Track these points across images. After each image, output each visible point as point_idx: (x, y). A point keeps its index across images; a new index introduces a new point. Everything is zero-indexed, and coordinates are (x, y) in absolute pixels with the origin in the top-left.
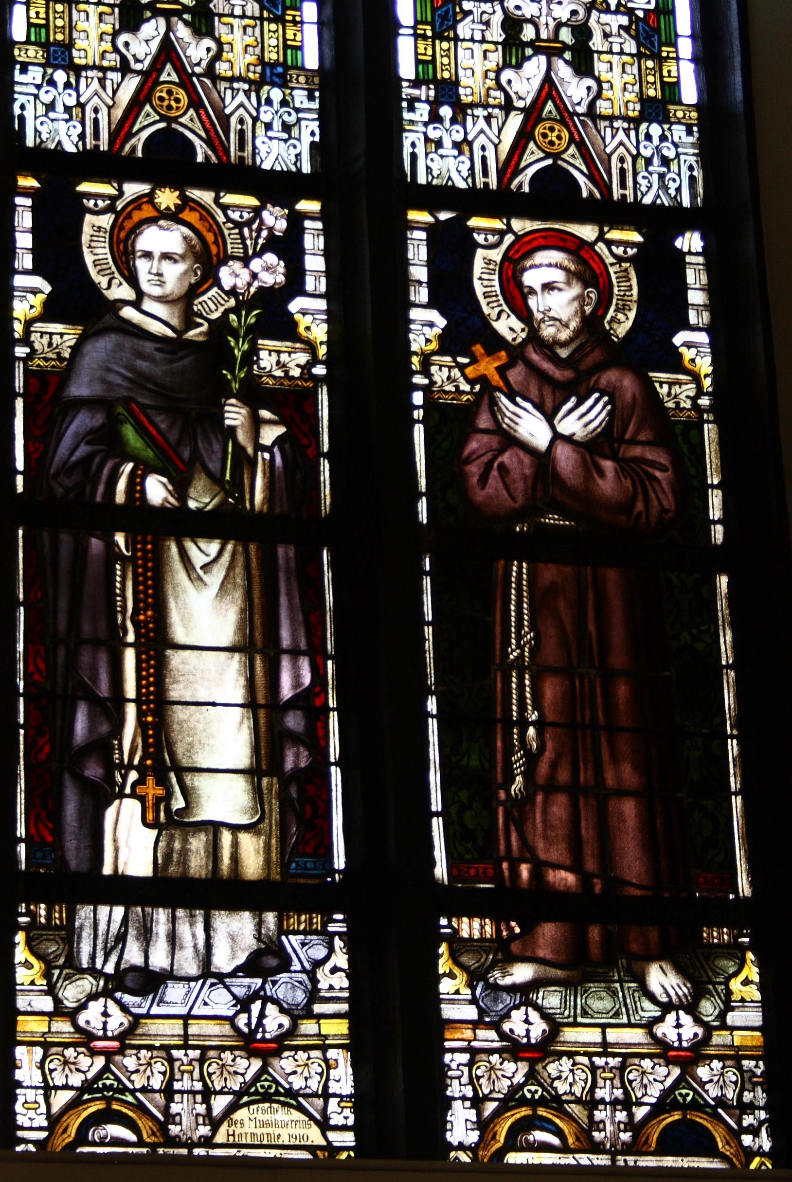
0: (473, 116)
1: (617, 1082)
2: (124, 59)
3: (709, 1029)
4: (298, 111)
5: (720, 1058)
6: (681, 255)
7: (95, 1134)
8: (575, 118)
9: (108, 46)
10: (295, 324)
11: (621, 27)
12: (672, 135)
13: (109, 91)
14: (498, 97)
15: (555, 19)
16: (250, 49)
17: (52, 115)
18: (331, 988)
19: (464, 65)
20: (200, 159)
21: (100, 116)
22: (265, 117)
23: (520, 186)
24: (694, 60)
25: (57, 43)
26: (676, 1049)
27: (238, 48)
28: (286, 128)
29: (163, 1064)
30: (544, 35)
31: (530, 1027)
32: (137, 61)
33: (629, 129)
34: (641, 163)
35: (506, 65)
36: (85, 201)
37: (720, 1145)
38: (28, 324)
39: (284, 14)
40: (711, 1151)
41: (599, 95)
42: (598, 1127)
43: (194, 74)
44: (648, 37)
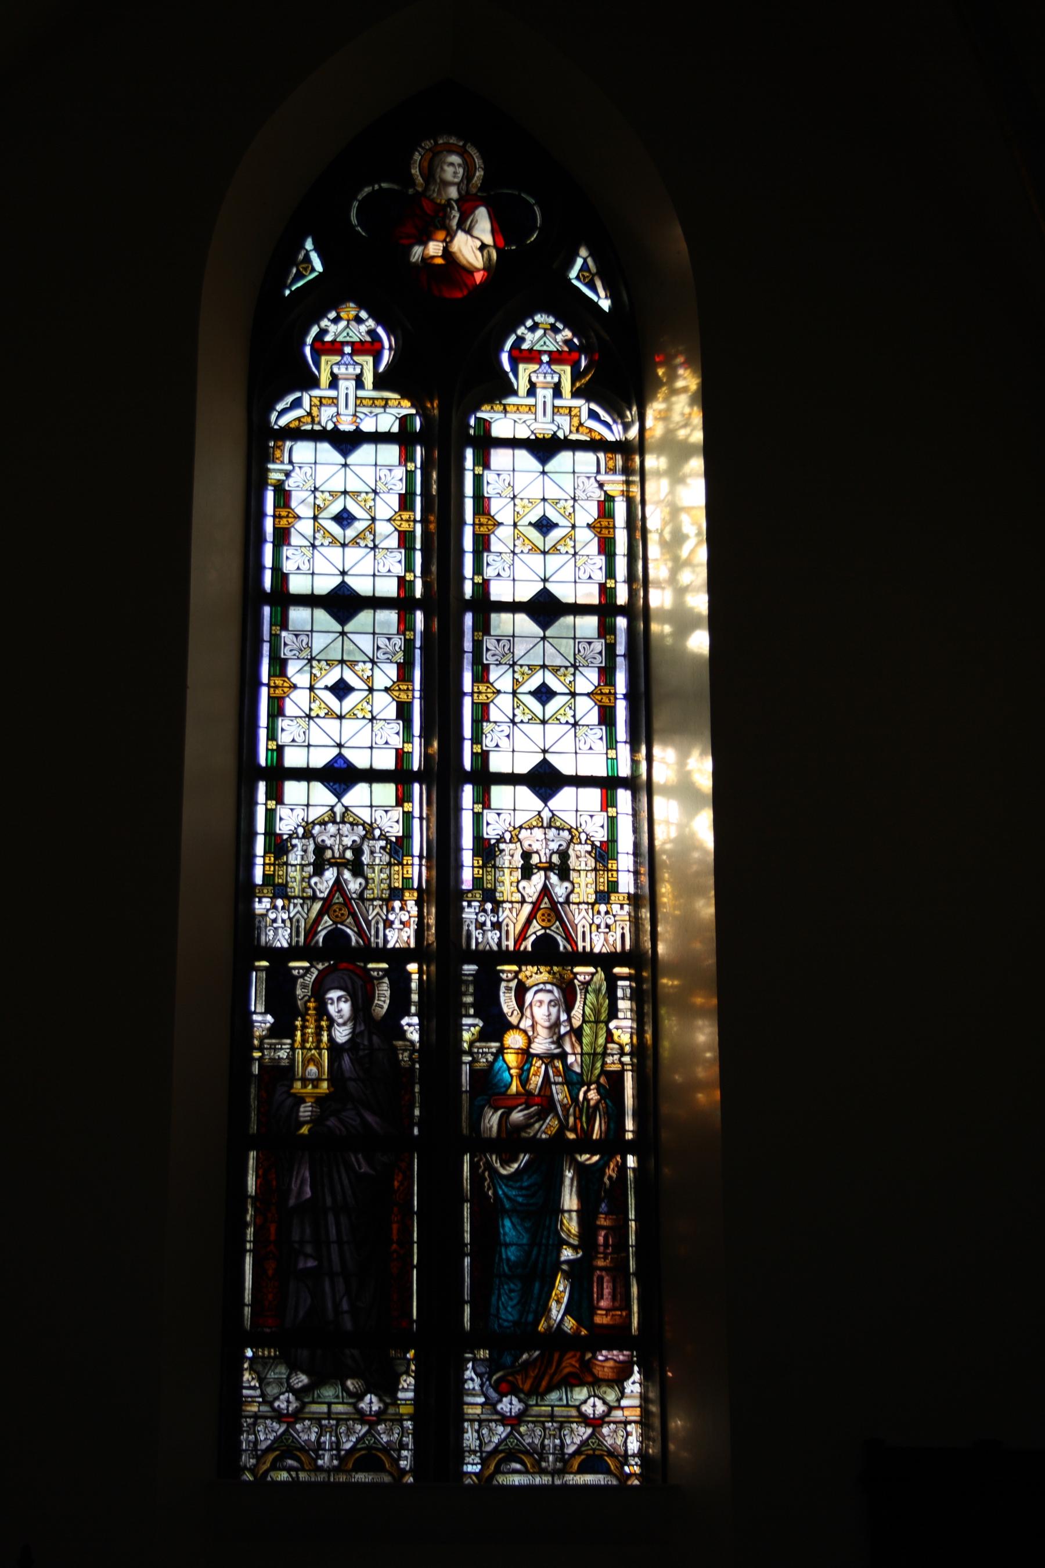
2: (523, 896)
3: (611, 1409)
4: (614, 916)
5: (309, 1419)
6: (410, 974)
10: (405, 1032)
13: (515, 914)
14: (517, 897)
20: (353, 943)
22: (597, 921)
23: (526, 948)
28: (608, 926)
30: (337, 855)
32: (321, 892)
34: (594, 927)
38: (262, 1039)
40: (607, 1471)
41: (365, 888)
43: (352, 898)
44: (397, 852)
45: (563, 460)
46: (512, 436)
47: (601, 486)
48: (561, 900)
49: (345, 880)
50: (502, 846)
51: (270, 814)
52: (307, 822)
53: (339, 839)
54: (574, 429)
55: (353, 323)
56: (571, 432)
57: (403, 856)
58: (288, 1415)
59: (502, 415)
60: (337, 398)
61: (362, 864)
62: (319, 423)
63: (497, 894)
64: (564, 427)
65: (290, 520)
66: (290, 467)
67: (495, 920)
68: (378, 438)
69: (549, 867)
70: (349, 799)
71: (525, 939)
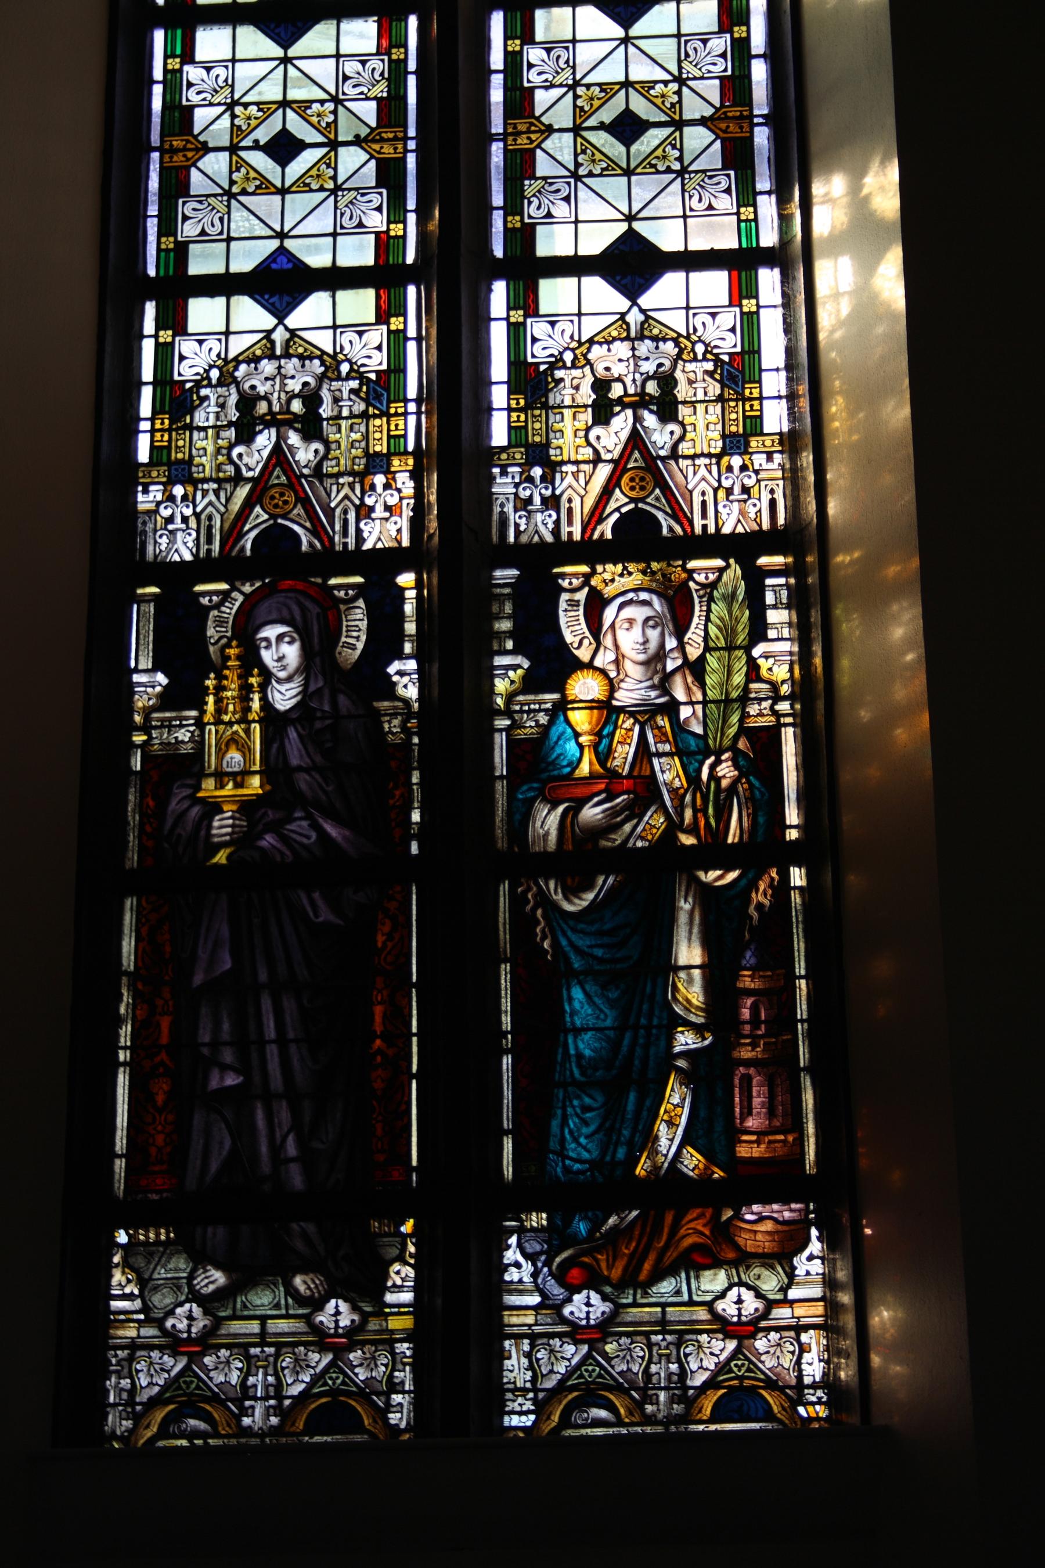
0: (562, 472)
1: (271, 1371)
2: (596, 452)
4: (757, 472)
7: (577, 1417)
8: (303, 481)
9: (582, 441)
11: (706, 372)
12: (752, 464)
14: (587, 453)
15: (642, 374)
16: (712, 427)
17: (170, 527)
18: (808, 1273)
19: (197, 446)
20: (305, 547)
21: (349, 516)
24: (490, 409)
25: (178, 462)
26: (734, 1324)
27: (701, 426)
29: (386, 1357)
30: (276, 408)
31: (591, 1309)
32: (250, 469)
33: (354, 482)
34: (721, 494)
35: (239, 441)
36: (560, 581)
37: (366, 1422)
38: (147, 712)
39: (388, 407)
41: (325, 457)
42: (651, 1400)
43: (303, 475)
49: (290, 447)
58: (189, 1341)
61: (676, 402)
67: (548, 493)
71: (601, 520)
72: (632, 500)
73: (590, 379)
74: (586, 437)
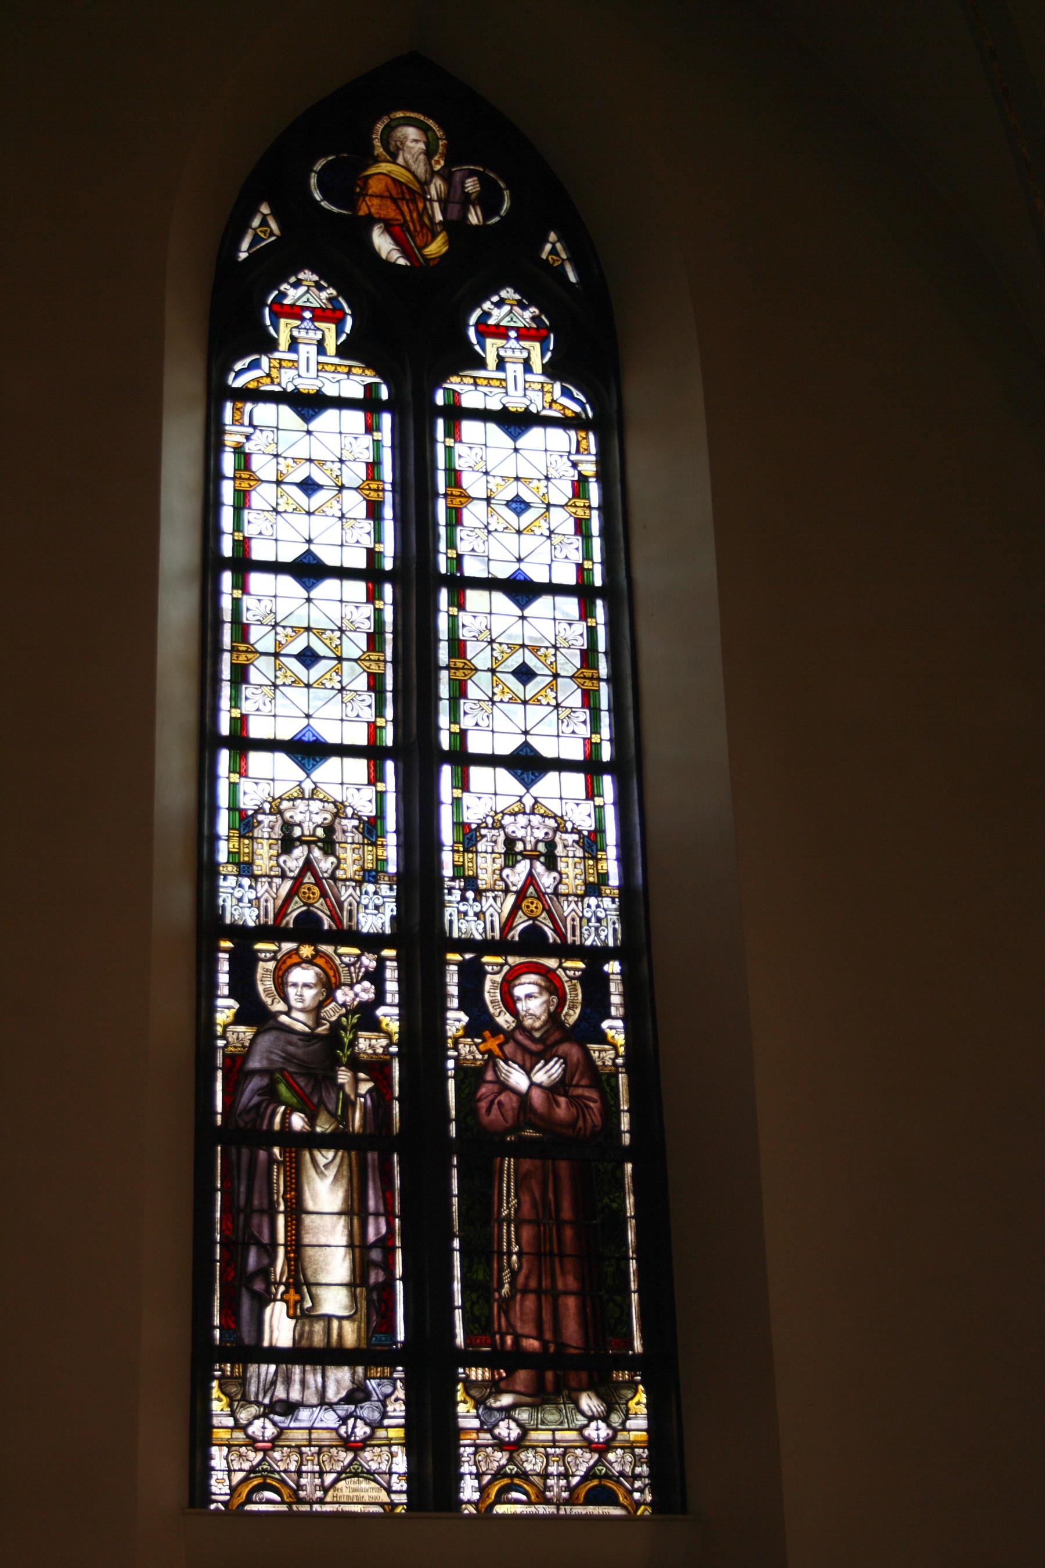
1: (561, 1463)
4: (605, 910)
5: (622, 1448)
7: (256, 1497)
14: (276, 871)
17: (241, 904)
22: (364, 901)
23: (513, 937)
30: (529, 847)
32: (291, 871)
34: (585, 921)
35: (506, 866)
38: (225, 1027)
41: (560, 882)
43: (324, 878)
44: (590, 847)
45: (535, 435)
46: (337, 395)
47: (575, 465)
48: (549, 891)
49: (539, 874)
50: (260, 817)
51: (233, 787)
52: (273, 798)
53: (530, 831)
54: (547, 405)
55: (516, 309)
56: (544, 408)
57: (377, 837)
58: (509, 1443)
59: (473, 388)
60: (505, 380)
61: (555, 857)
62: (279, 384)
63: (479, 882)
64: (537, 404)
65: (252, 483)
66: (251, 430)
67: (478, 909)
68: (342, 403)
69: (533, 858)
70: (537, 789)
71: (512, 928)
72: (305, 904)
73: (280, 822)
74: (501, 875)
